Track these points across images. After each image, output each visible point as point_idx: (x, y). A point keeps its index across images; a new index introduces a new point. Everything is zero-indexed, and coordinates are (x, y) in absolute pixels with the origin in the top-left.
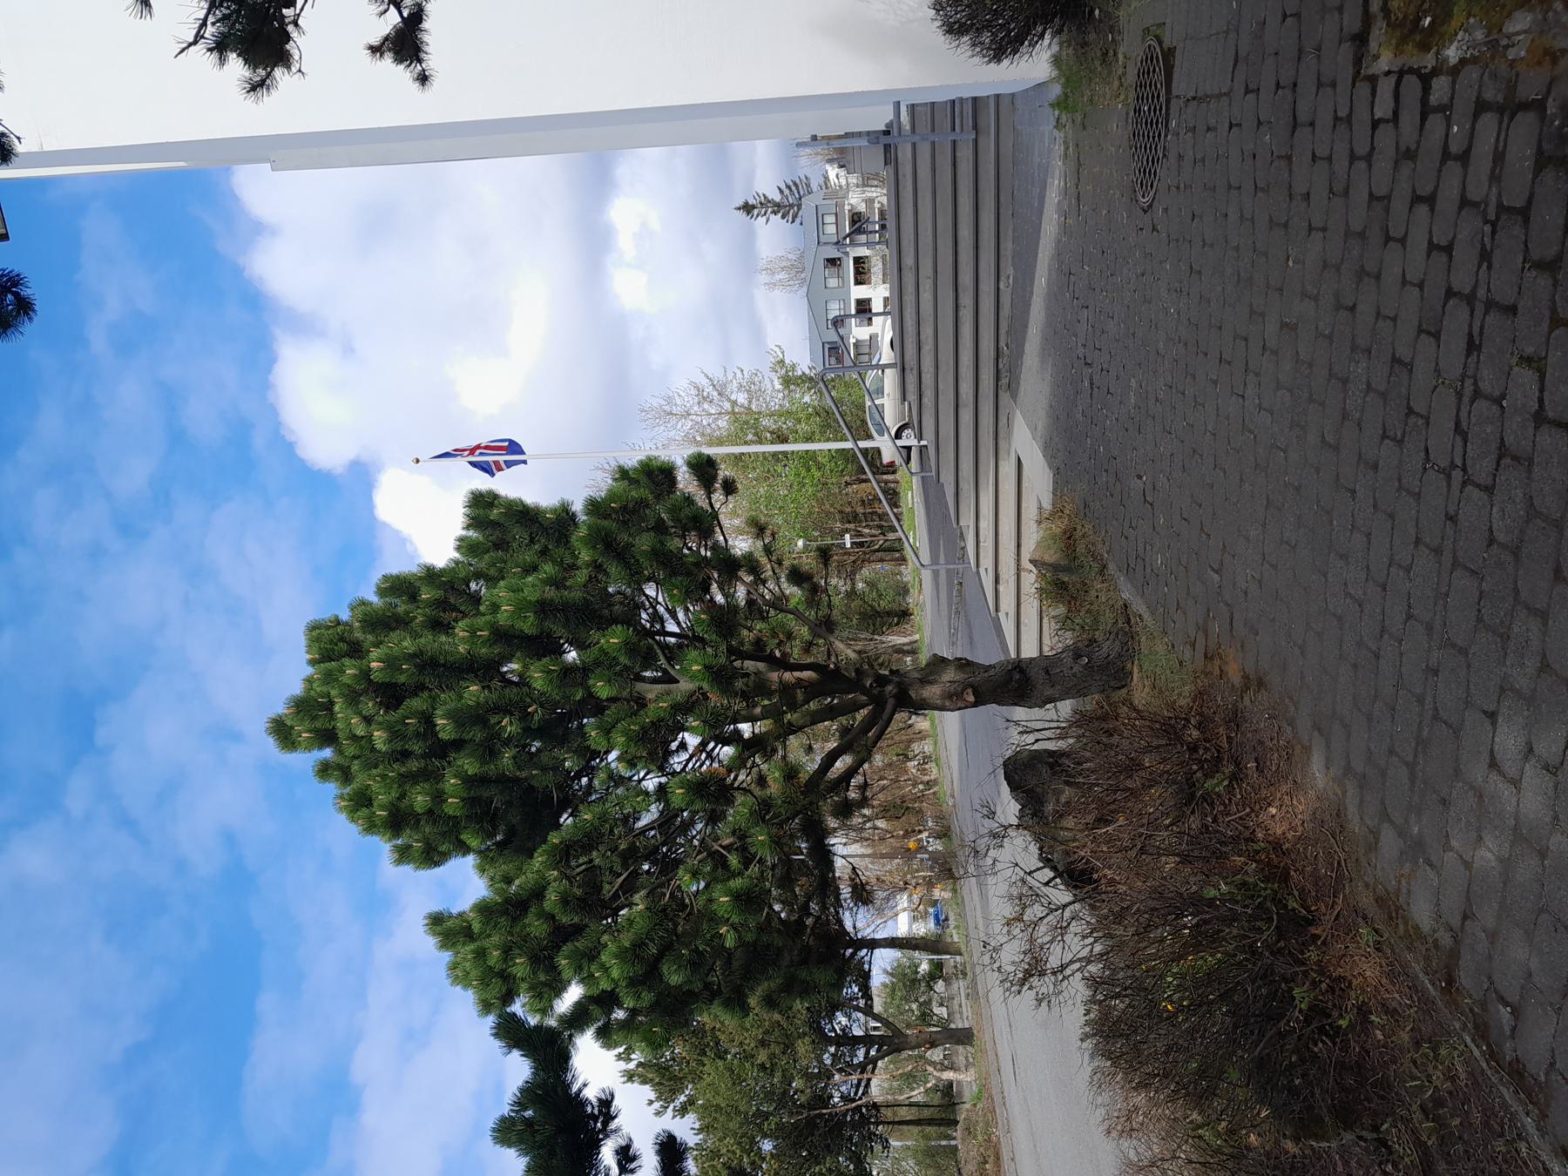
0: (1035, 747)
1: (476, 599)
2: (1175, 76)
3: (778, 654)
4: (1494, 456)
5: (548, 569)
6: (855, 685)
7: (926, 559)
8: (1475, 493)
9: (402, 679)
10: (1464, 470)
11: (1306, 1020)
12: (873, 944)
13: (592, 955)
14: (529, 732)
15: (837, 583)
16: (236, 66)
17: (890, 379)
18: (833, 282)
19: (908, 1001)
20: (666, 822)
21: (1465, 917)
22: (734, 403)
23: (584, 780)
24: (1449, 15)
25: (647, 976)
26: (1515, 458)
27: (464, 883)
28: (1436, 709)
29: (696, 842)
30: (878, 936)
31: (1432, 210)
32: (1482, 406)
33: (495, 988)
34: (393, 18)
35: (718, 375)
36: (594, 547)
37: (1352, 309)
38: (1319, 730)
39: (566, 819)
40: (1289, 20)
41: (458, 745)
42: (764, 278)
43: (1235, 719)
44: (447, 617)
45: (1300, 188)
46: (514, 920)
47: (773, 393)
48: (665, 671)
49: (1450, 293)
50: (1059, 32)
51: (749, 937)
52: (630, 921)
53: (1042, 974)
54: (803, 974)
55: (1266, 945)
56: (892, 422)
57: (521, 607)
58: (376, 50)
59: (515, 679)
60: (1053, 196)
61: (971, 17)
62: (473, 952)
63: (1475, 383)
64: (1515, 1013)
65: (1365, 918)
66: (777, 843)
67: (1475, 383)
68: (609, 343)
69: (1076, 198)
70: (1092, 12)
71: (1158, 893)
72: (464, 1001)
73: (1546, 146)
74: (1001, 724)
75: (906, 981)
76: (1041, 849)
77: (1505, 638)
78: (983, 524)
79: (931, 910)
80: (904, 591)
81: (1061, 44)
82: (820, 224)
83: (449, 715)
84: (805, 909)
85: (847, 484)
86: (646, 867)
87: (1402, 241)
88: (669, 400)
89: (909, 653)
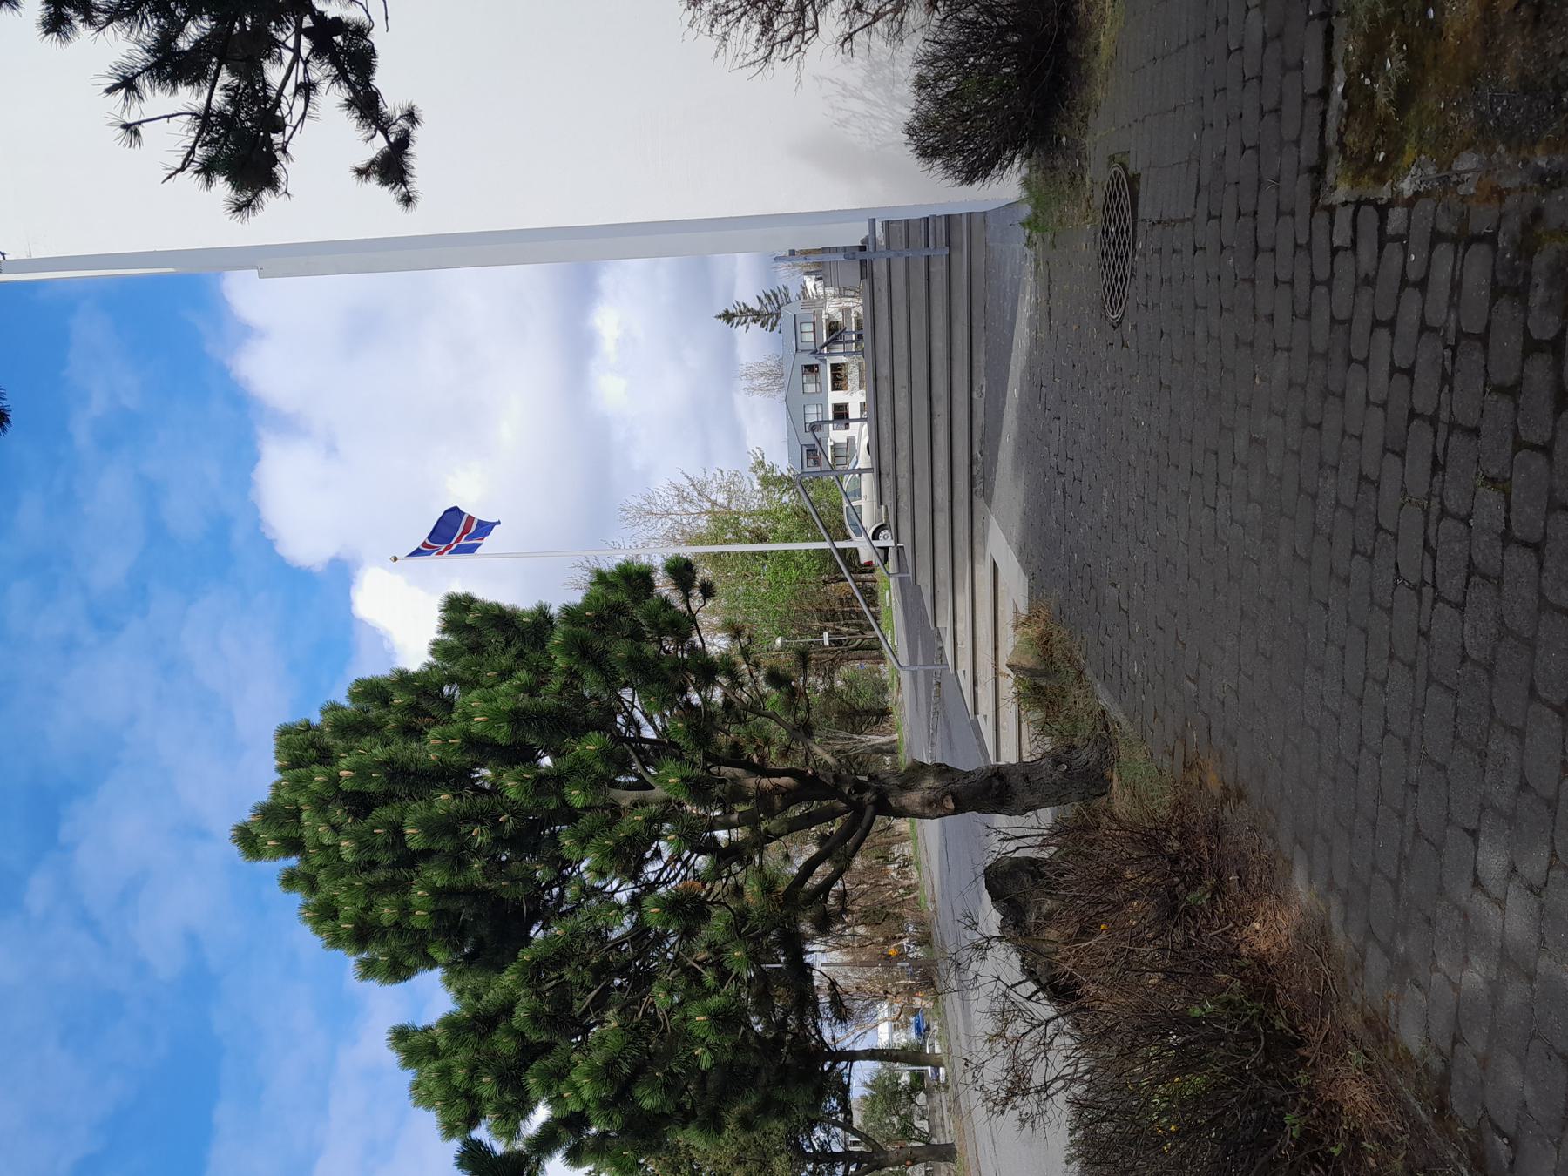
0: (1016, 855)
1: (449, 704)
2: (1141, 201)
3: (755, 759)
4: (1463, 574)
5: (522, 675)
6: (833, 791)
7: (904, 660)
8: (1448, 610)
9: (372, 787)
10: (1434, 587)
11: (1297, 1145)
12: (852, 1056)
13: (561, 1074)
14: (498, 841)
15: (816, 681)
16: (222, 188)
17: (867, 483)
18: (811, 388)
19: (888, 1113)
20: (640, 934)
21: (1455, 1042)
22: (714, 503)
23: (556, 890)
24: (1401, 152)
25: (620, 1096)
26: (1485, 576)
27: (431, 997)
28: (1417, 825)
29: (670, 956)
30: (858, 1047)
31: (1393, 334)
32: (1448, 523)
33: (461, 1110)
34: (380, 143)
35: (698, 475)
36: (570, 655)
37: (1319, 426)
38: (1301, 843)
39: (536, 932)
40: (1248, 152)
41: (426, 854)
42: (743, 383)
43: (1216, 830)
44: (420, 722)
45: (1264, 310)
46: (482, 1037)
47: (753, 494)
48: (640, 776)
49: (1413, 414)
50: (1029, 156)
51: (727, 1057)
52: (602, 1039)
53: (1026, 1092)
54: (780, 1094)
55: (1255, 1068)
56: (869, 524)
57: (495, 717)
58: (362, 173)
59: (487, 786)
60: (1024, 311)
61: (942, 142)
62: (438, 1070)
63: (1442, 503)
64: (1513, 1143)
65: (1354, 1040)
66: (753, 959)
67: (1442, 503)
68: (593, 445)
69: (1047, 313)
70: (1059, 139)
71: (1141, 1010)
72: (428, 1121)
73: (1500, 277)
74: (982, 829)
75: (887, 1095)
76: (1023, 960)
77: (1483, 755)
78: (960, 627)
79: (912, 1019)
80: (882, 689)
81: (1030, 167)
82: (798, 332)
83: (419, 824)
84: (783, 1024)
85: (825, 582)
86: (618, 981)
87: (1365, 363)
88: (650, 500)
89: (887, 752)
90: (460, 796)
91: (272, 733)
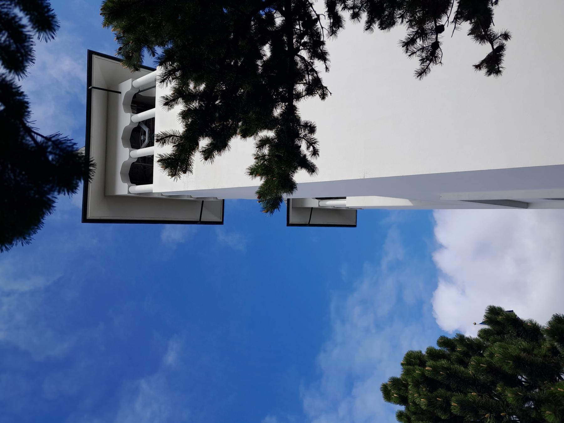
57: (506, 357)
90: (482, 396)
91: (406, 353)
